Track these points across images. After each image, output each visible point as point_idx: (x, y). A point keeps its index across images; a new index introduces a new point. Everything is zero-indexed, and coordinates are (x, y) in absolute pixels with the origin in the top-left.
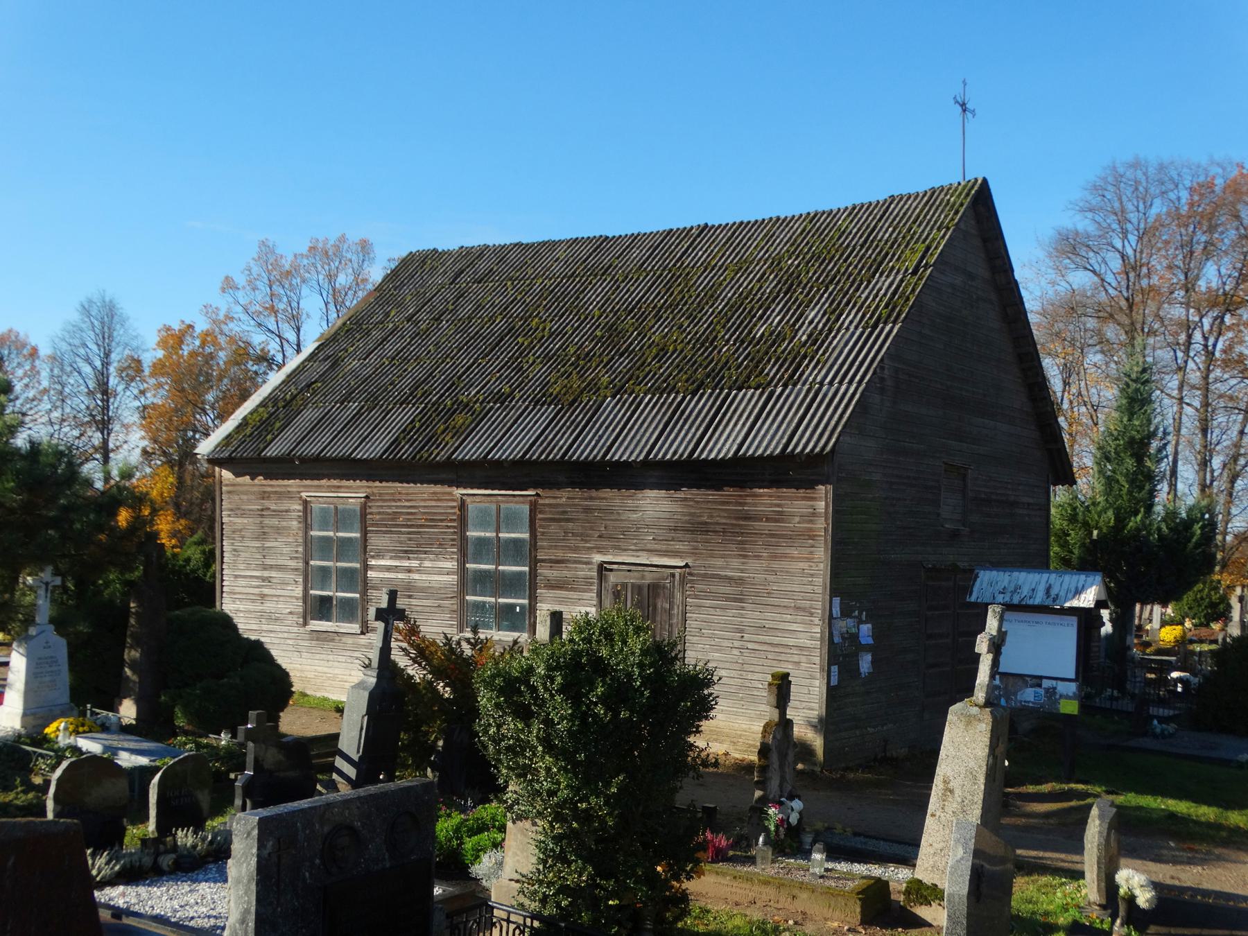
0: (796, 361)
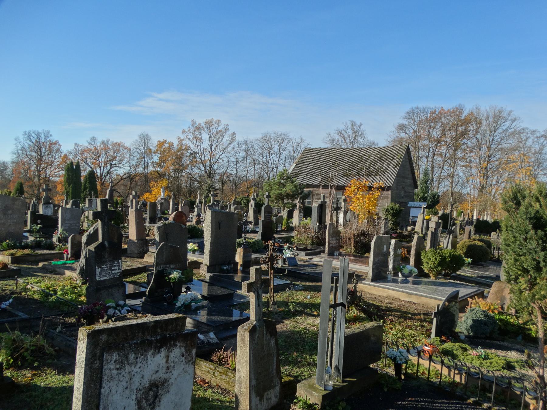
0: (384, 171)
